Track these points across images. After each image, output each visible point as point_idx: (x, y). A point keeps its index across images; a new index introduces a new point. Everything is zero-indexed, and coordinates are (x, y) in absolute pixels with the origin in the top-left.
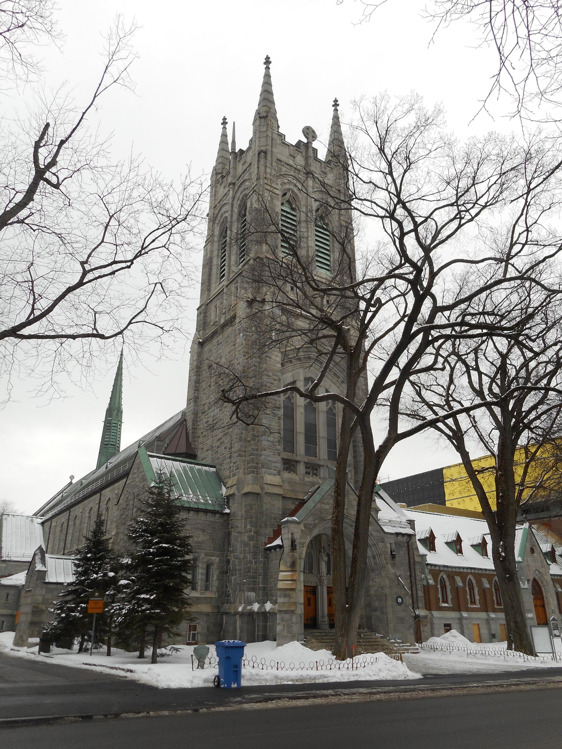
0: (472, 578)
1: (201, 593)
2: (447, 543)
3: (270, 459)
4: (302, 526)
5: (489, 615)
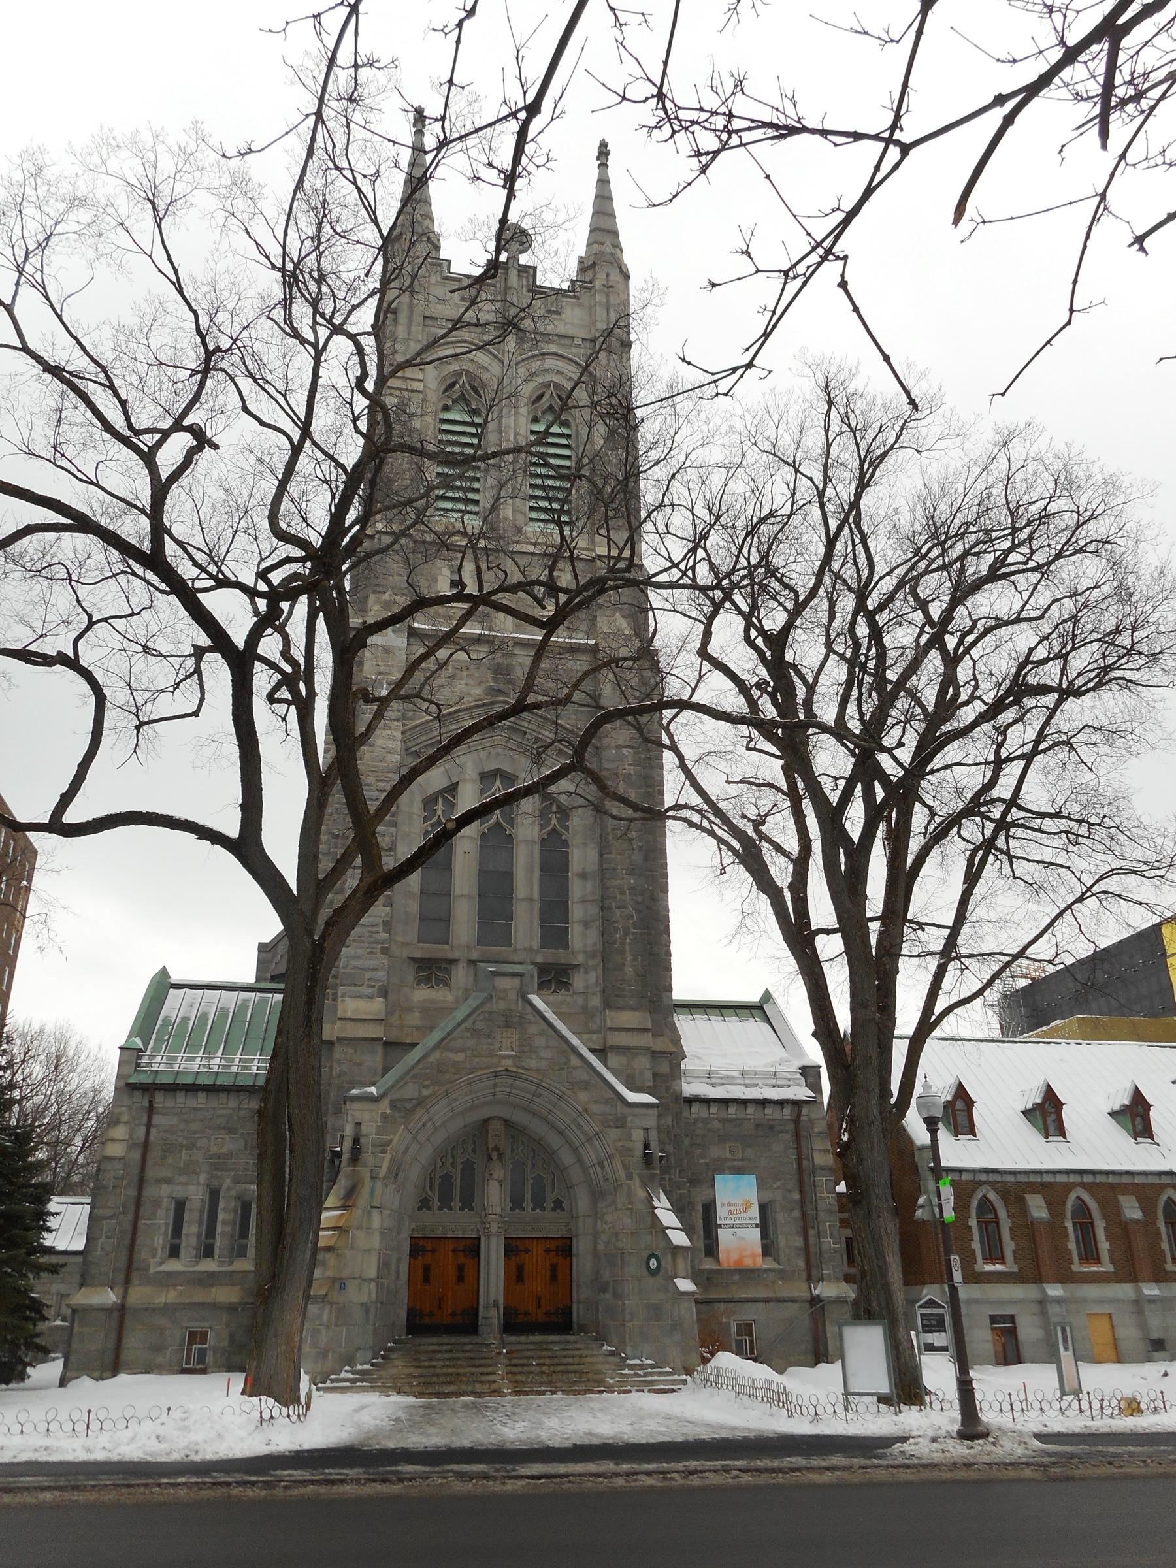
0: (1086, 1197)
1: (221, 1263)
2: (1112, 1114)
3: (358, 963)
4: (385, 1107)
5: (1139, 1292)
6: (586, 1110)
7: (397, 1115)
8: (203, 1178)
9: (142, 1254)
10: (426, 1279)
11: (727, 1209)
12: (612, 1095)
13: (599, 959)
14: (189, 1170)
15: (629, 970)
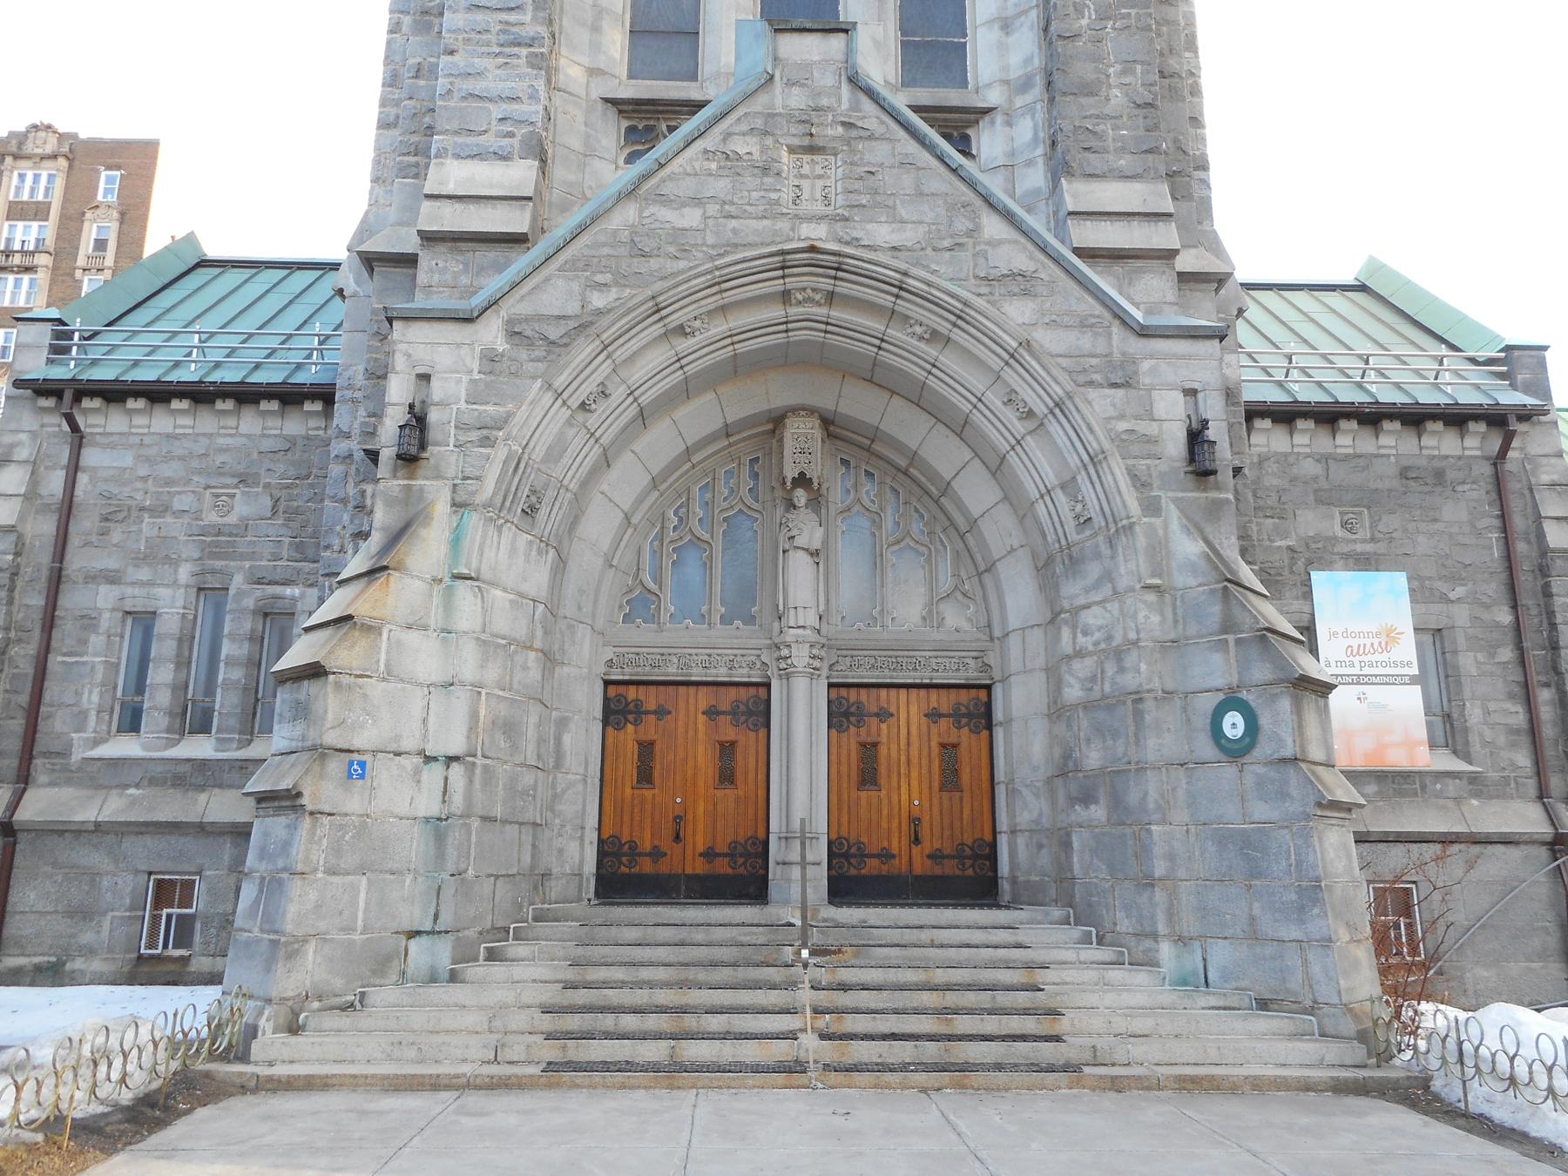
6: (1027, 344)
7: (523, 355)
8: (184, 573)
9: (56, 724)
10: (645, 776)
11: (1343, 643)
12: (1098, 309)
13: (1038, 90)
14: (157, 555)
15: (1118, 98)
